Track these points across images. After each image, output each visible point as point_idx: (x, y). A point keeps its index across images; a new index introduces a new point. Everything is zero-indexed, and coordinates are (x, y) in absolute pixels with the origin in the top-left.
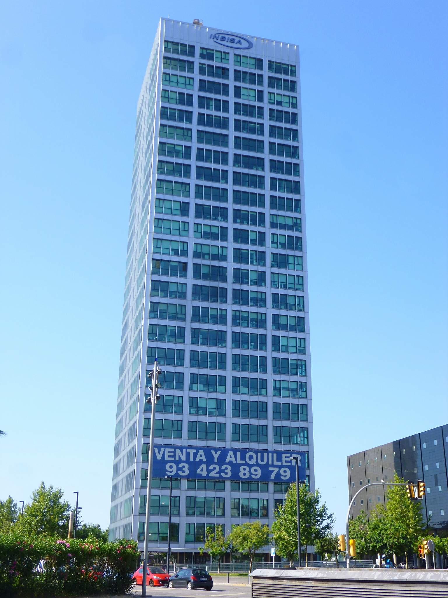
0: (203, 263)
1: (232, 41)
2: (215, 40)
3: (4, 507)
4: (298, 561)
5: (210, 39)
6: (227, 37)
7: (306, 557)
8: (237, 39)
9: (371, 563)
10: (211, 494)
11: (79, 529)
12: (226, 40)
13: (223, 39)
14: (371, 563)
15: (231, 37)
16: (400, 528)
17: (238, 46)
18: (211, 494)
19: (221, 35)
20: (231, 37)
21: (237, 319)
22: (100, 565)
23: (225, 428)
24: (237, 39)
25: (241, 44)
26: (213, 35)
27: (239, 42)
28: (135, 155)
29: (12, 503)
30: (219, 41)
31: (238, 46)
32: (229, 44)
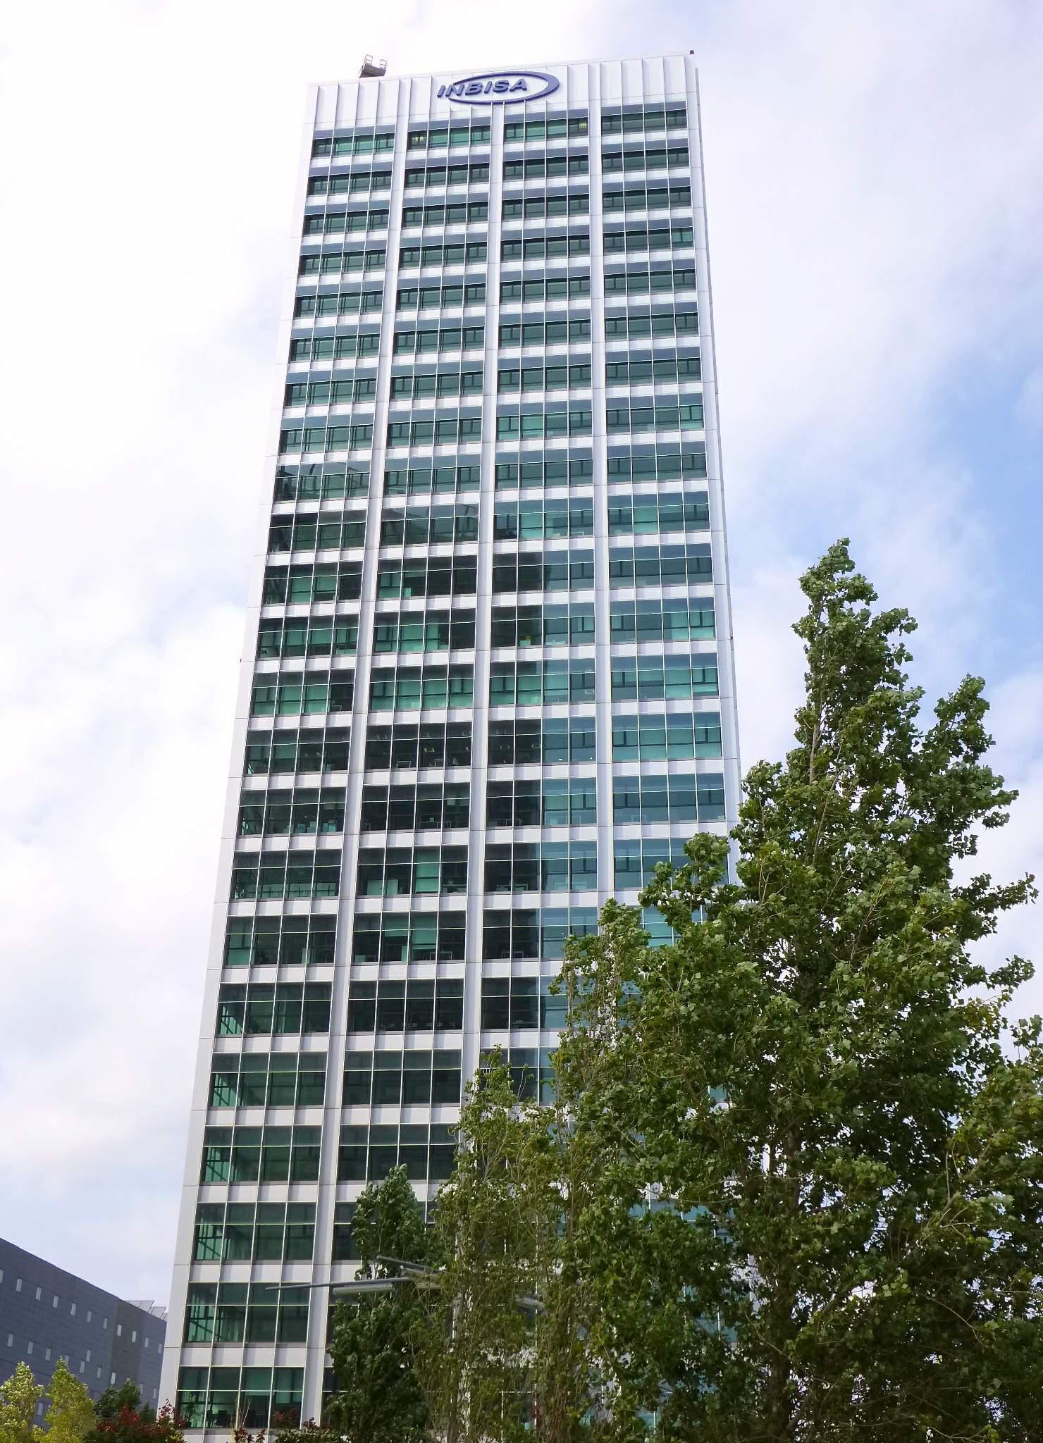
1: (501, 88)
2: (454, 96)
3: (380, 1351)
6: (485, 83)
8: (513, 81)
9: (561, 693)
11: (856, 1298)
13: (474, 91)
14: (561, 693)
15: (495, 81)
16: (546, 1322)
17: (520, 95)
20: (495, 81)
21: (399, 386)
24: (513, 81)
25: (525, 89)
26: (447, 87)
27: (520, 87)
30: (464, 98)
31: (520, 95)
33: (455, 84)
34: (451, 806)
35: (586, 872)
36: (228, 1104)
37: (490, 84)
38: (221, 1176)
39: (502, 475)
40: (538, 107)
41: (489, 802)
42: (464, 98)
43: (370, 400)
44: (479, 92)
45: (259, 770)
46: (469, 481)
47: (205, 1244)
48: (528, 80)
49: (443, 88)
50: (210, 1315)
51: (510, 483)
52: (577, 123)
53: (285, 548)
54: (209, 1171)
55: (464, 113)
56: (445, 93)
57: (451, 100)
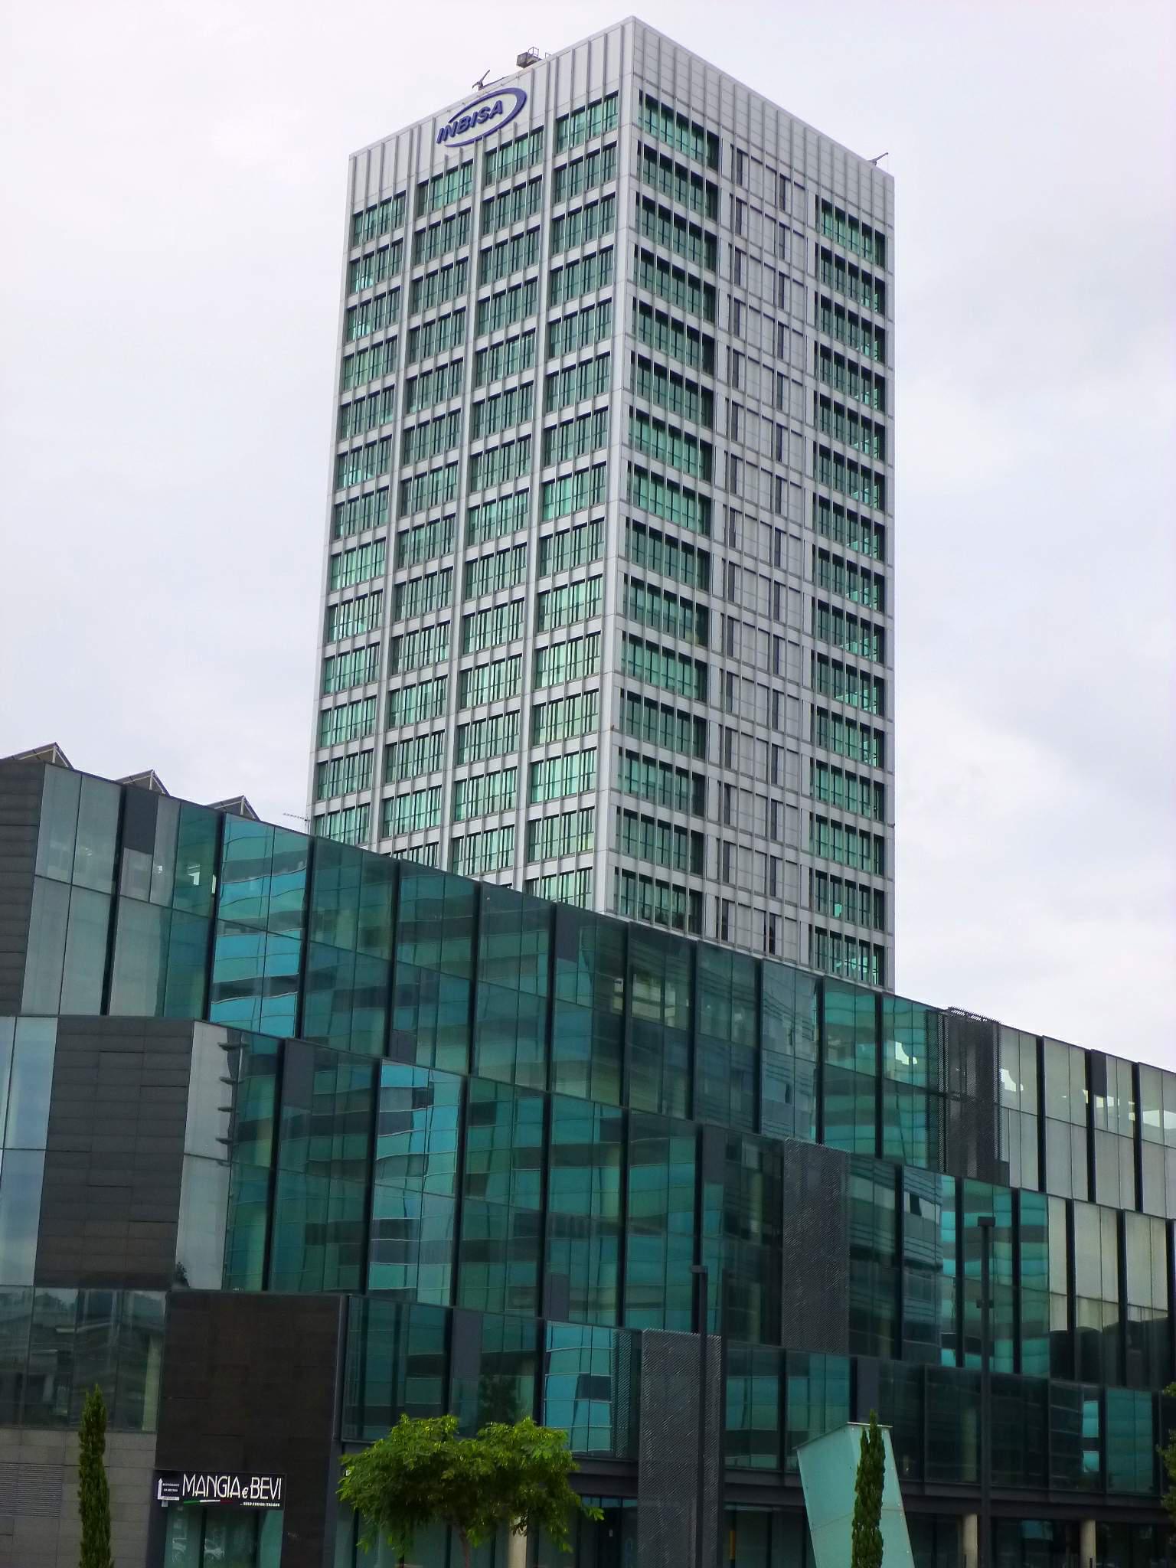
1: (485, 116)
13: (465, 125)
15: (477, 109)
17: (498, 120)
27: (499, 109)
31: (498, 120)
56: (444, 135)
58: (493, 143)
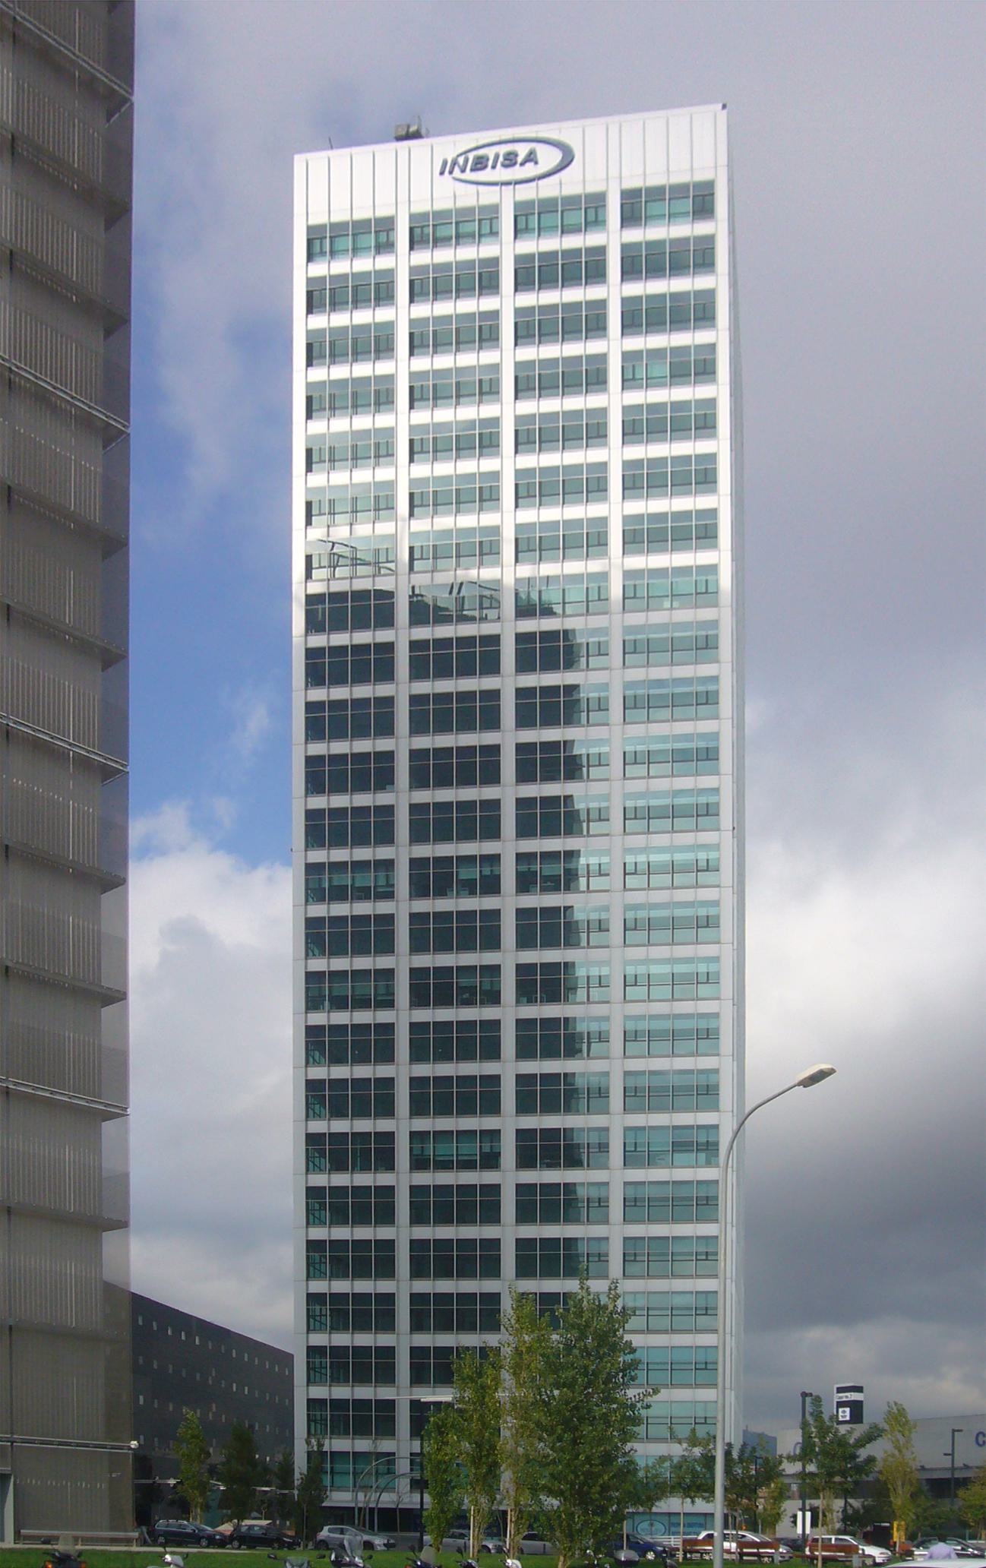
0: (641, 1281)
1: (510, 160)
4: (312, 1403)
5: (442, 177)
6: (490, 152)
7: (98, 1548)
8: (522, 150)
10: (340, 266)
12: (490, 163)
13: (480, 164)
15: (503, 149)
17: (530, 170)
18: (340, 266)
19: (471, 156)
20: (503, 149)
22: (543, 1410)
23: (661, 666)
24: (522, 150)
27: (531, 158)
28: (117, 444)
29: (717, 1144)
31: (530, 170)
32: (502, 174)
33: (458, 156)
34: (485, 876)
35: (600, 930)
36: (321, 1170)
37: (497, 157)
38: (319, 1219)
39: (522, 492)
40: (548, 189)
41: (518, 707)
42: (469, 175)
43: (388, 464)
44: (486, 167)
45: (321, 899)
46: (490, 393)
47: (313, 1215)
48: (541, 150)
49: (445, 163)
50: (323, 459)
51: (529, 340)
52: (591, 209)
53: (321, 845)
54: (311, 1217)
55: (468, 197)
57: (456, 179)
58: (526, 193)
